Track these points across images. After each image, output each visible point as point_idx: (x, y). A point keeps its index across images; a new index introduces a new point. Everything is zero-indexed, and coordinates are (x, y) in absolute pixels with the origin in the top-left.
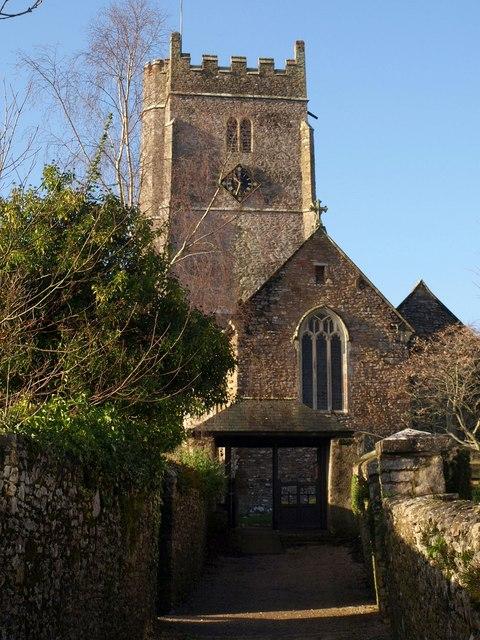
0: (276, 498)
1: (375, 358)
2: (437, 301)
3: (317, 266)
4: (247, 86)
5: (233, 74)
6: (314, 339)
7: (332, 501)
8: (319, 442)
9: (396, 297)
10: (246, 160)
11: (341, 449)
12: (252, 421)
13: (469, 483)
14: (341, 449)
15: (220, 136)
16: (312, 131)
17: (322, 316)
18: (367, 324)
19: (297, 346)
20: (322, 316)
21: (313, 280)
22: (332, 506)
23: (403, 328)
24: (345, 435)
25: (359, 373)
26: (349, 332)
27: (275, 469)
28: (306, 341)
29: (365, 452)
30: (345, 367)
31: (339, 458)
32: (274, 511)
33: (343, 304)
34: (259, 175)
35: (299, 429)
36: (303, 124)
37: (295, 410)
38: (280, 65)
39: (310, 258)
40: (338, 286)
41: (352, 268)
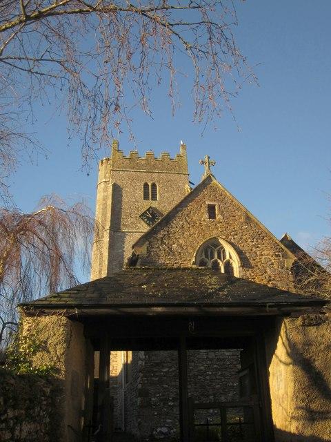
4: (154, 166)
10: (154, 204)
15: (141, 193)
21: (206, 215)
23: (285, 256)
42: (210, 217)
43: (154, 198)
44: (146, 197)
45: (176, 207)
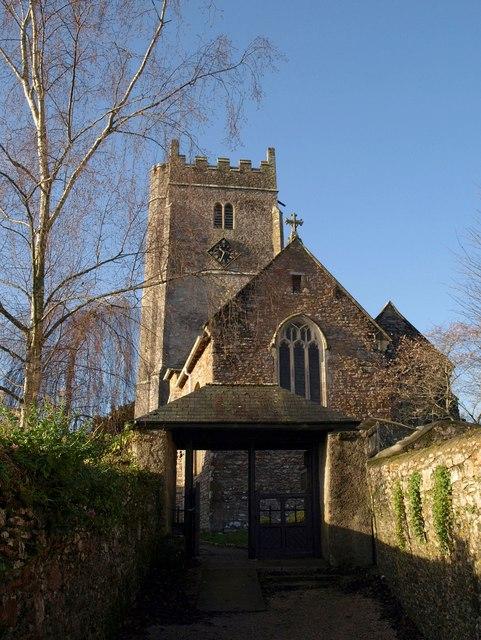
0: (253, 518)
1: (354, 367)
2: (405, 321)
3: (293, 276)
4: (231, 179)
5: (219, 170)
6: (291, 347)
7: (331, 519)
8: (307, 439)
9: (374, 311)
10: (229, 235)
11: (342, 446)
12: (220, 410)
13: (182, 524)
14: (342, 446)
15: (210, 217)
16: (281, 213)
17: (299, 325)
18: (345, 333)
19: (275, 354)
20: (299, 325)
21: (290, 289)
22: (332, 527)
23: (380, 337)
24: (347, 428)
25: (338, 381)
26: (327, 340)
27: (251, 480)
28: (283, 350)
29: (382, 448)
30: (323, 375)
31: (341, 459)
32: (249, 528)
33: (321, 312)
34: (239, 246)
35: (286, 419)
36: (274, 208)
37: (277, 396)
38: (256, 164)
39: (287, 267)
40: (314, 294)
41: (328, 278)
42: (294, 290)
43: (229, 225)
44: (217, 223)
45: (203, 350)
